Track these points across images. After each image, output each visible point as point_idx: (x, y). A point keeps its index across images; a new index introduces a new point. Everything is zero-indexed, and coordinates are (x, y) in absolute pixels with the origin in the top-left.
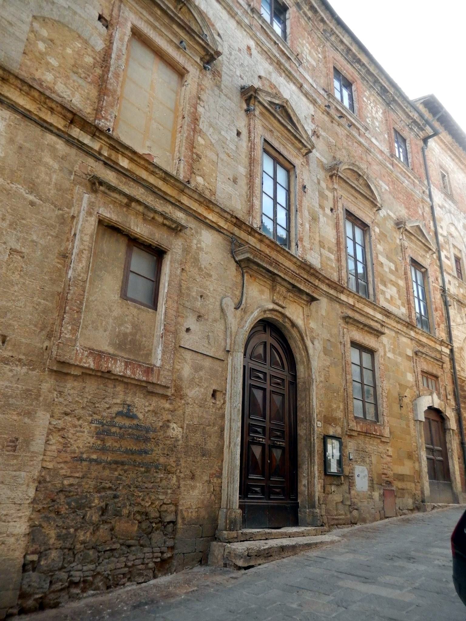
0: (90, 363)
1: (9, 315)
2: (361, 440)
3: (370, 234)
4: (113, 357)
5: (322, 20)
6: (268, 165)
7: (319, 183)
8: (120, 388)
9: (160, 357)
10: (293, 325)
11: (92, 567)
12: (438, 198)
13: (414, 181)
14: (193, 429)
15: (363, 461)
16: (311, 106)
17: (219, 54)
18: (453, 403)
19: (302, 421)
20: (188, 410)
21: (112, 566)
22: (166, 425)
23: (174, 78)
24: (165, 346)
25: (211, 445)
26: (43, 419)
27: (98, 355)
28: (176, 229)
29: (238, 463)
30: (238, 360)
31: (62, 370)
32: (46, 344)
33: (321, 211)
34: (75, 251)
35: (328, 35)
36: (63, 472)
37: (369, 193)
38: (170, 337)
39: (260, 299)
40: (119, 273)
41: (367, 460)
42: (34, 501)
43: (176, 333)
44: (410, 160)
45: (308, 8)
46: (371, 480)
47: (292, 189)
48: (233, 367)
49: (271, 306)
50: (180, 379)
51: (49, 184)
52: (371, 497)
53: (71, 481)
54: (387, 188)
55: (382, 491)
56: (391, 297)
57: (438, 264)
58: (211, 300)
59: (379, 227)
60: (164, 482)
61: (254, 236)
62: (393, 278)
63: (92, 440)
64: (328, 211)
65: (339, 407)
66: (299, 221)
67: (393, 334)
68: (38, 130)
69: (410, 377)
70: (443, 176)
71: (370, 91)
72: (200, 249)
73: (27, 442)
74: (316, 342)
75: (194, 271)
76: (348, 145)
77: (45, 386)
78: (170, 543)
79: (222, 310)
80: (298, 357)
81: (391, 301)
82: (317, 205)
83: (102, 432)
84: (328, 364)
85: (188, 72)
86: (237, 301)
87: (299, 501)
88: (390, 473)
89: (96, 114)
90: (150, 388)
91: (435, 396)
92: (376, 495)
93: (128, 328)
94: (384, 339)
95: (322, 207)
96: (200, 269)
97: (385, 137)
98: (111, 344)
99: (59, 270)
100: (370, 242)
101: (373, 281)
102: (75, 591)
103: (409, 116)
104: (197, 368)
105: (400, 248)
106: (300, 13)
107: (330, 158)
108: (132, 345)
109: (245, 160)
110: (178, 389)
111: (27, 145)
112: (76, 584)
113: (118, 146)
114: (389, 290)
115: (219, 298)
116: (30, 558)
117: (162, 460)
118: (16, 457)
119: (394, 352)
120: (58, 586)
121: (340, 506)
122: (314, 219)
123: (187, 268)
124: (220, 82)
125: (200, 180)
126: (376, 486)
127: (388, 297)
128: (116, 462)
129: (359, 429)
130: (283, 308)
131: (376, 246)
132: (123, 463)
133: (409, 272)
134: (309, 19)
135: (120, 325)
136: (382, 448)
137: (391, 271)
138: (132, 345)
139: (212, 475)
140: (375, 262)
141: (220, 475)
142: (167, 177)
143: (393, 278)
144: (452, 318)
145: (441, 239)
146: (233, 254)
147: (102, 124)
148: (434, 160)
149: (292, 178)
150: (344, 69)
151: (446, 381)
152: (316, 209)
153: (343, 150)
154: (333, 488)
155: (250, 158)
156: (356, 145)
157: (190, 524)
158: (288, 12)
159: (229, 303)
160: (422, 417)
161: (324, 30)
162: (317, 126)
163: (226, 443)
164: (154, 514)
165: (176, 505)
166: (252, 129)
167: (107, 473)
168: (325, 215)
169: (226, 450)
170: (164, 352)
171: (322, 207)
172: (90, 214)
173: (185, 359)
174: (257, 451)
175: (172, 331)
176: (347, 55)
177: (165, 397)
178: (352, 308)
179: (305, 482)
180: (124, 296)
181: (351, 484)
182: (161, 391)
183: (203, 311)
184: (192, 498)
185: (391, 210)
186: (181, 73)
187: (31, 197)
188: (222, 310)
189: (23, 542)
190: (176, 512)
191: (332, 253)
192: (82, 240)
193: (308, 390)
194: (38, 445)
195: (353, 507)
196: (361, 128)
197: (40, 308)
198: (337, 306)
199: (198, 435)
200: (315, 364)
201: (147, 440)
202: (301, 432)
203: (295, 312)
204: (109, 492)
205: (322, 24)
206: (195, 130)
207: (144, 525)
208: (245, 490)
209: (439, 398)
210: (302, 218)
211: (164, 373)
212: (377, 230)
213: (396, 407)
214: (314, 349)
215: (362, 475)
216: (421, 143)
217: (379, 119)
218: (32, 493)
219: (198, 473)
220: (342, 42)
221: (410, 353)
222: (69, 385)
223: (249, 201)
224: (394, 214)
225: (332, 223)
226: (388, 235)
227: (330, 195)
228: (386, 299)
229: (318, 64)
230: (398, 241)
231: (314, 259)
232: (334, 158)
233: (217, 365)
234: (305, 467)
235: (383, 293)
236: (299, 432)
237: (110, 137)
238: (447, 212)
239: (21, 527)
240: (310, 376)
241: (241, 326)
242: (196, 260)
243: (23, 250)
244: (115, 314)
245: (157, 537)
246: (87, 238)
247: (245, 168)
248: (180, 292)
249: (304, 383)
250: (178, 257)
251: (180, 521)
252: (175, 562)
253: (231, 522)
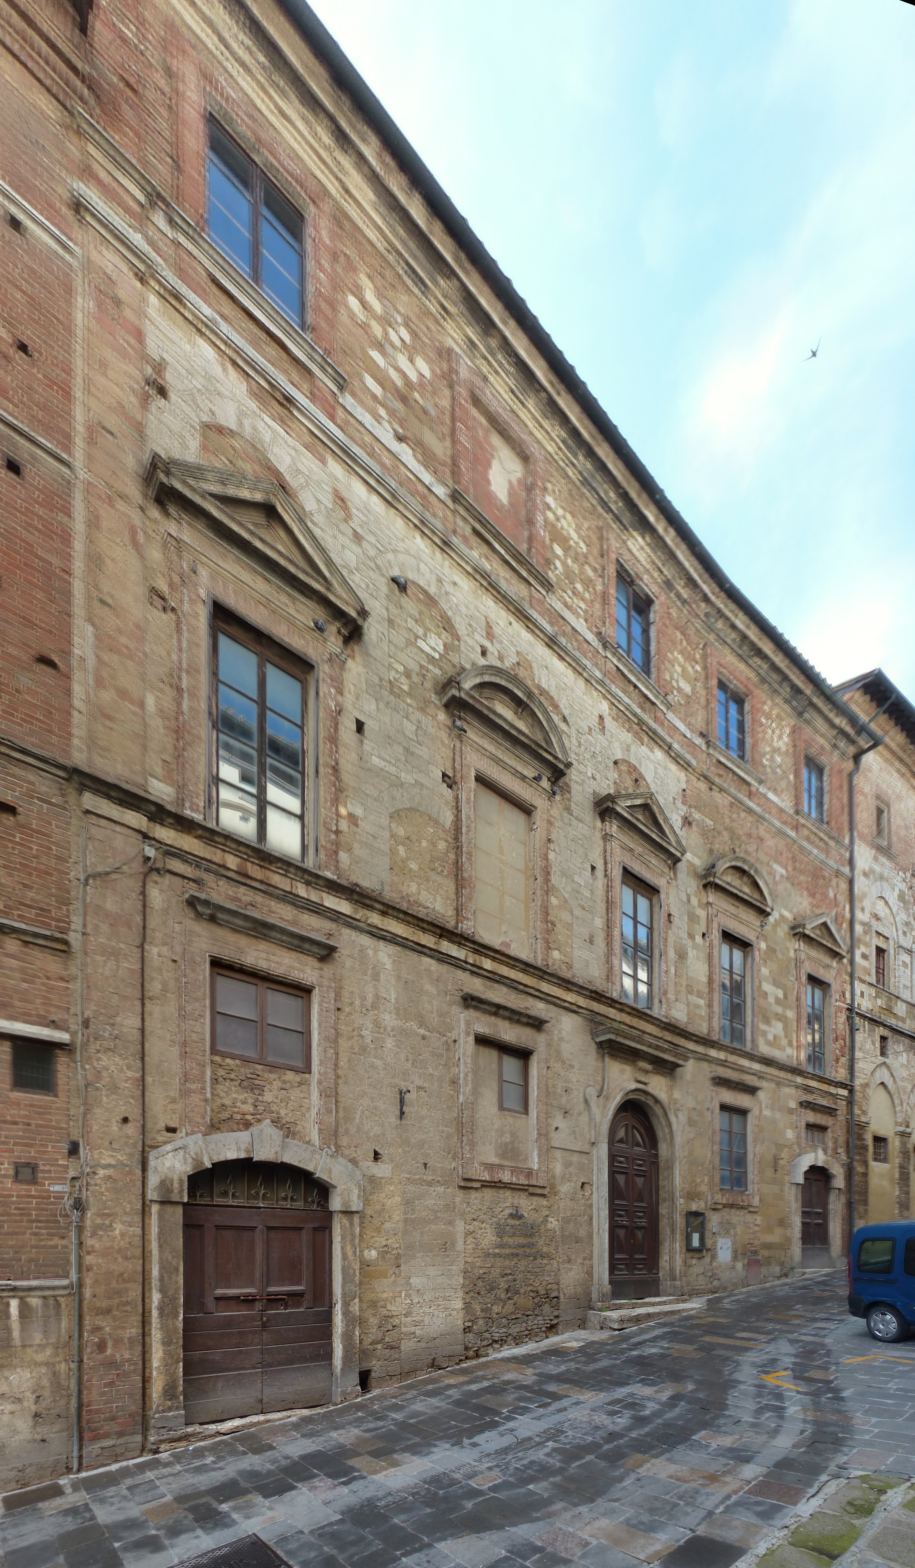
0: (486, 1176)
1: (426, 1146)
2: (726, 1214)
3: (753, 956)
4: (501, 1167)
5: (706, 599)
6: (627, 894)
7: (689, 901)
8: (508, 1193)
9: (536, 1160)
10: (657, 1101)
11: (504, 1330)
12: (864, 856)
13: (827, 844)
14: (566, 1221)
15: (727, 1232)
16: (682, 775)
17: (569, 765)
18: (844, 1157)
19: (664, 1200)
20: (562, 1205)
21: (517, 1330)
22: (545, 1220)
23: (519, 817)
24: (540, 1149)
25: (582, 1233)
26: (460, 1226)
27: (490, 1167)
28: (537, 1024)
29: (607, 1246)
30: (603, 1150)
31: (467, 1185)
32: (454, 1165)
33: (689, 943)
34: (462, 1076)
35: (713, 620)
36: (478, 1264)
37: (756, 896)
38: (543, 1140)
39: (623, 1079)
40: (495, 1085)
41: (732, 1232)
42: (463, 1286)
43: (546, 1135)
44: (826, 807)
45: (682, 583)
46: (735, 1252)
47: (655, 926)
48: (599, 1158)
49: (634, 1086)
50: (554, 1177)
51: (432, 1012)
52: (733, 1268)
53: (485, 1270)
54: (784, 872)
55: (746, 1261)
56: (775, 1037)
57: (849, 970)
58: (575, 1093)
59: (765, 941)
60: (548, 1267)
61: (613, 1007)
62: (779, 1010)
63: (494, 1238)
64: (699, 939)
65: (703, 1181)
66: (664, 968)
67: (773, 1086)
68: (414, 956)
69: (790, 1134)
70: (880, 812)
71: (772, 700)
72: (561, 1039)
73: (453, 1244)
74: (680, 1115)
75: (557, 1066)
76: (732, 820)
77: (458, 1199)
78: (556, 1313)
79: (586, 1101)
80: (660, 1134)
81: (774, 1043)
82: (686, 936)
83: (500, 1231)
84: (692, 1136)
85: (536, 808)
86: (598, 1087)
87: (660, 1274)
88: (756, 1242)
89: (457, 915)
90: (531, 1190)
91: (820, 1152)
92: (739, 1265)
93: (507, 1138)
94: (761, 1094)
95: (691, 936)
96: (563, 1062)
97: (789, 782)
98: (497, 1155)
99: (452, 1096)
100: (752, 968)
101: (752, 1022)
102: (496, 1346)
103: (833, 725)
104: (567, 1164)
105: (793, 963)
106: (670, 598)
107: (705, 856)
108: (510, 1151)
109: (601, 907)
110: (553, 1187)
111: (410, 977)
112: (496, 1342)
113: (482, 949)
114: (772, 1029)
115: (582, 1089)
116: (467, 1324)
117: (545, 1249)
118: (448, 1256)
119: (772, 1108)
120: (485, 1343)
121: (701, 1278)
122: (682, 956)
123: (551, 1064)
124: (569, 800)
125: (556, 954)
126: (739, 1257)
127: (770, 1037)
128: (513, 1254)
129: (724, 1202)
130: (645, 1084)
131: (759, 970)
132: (517, 1255)
133: (803, 996)
134: (684, 602)
135: (502, 1136)
136: (749, 1217)
137: (778, 1001)
138: (510, 1151)
139: (585, 1259)
140: (756, 995)
141: (591, 1259)
142: (527, 967)
143: (779, 1010)
144: (858, 1045)
145: (858, 929)
146: (594, 1034)
147: (466, 927)
148: (867, 789)
149: (656, 909)
150: (735, 678)
151: (837, 1129)
152: (684, 942)
153: (725, 833)
154: (694, 1261)
155: (607, 902)
156: (743, 814)
157: (570, 1298)
158: (652, 609)
159: (592, 1092)
160: (801, 1180)
161: (707, 615)
162: (690, 807)
163: (595, 1230)
164: (543, 1292)
165: (558, 1284)
166: (608, 857)
167: (507, 1262)
168: (695, 946)
169: (595, 1236)
170: (539, 1156)
171: (691, 936)
172: (468, 1034)
173: (555, 1158)
174: (621, 1233)
175: (543, 1134)
176: (740, 647)
177: (544, 1196)
178: (723, 1063)
179: (666, 1258)
180: (501, 1108)
181: (714, 1257)
182: (539, 1191)
183: (568, 1107)
184: (570, 1279)
185: (786, 908)
186: (527, 810)
187: (422, 1031)
188: (586, 1101)
189: (461, 1314)
190: (558, 1289)
191: (702, 998)
192: (465, 1063)
193: (670, 1168)
194: (460, 1245)
195: (713, 1277)
196: (753, 782)
197: (445, 1135)
198: (705, 1065)
199: (571, 1225)
200: (678, 1139)
201: (531, 1235)
202: (663, 1210)
203: (657, 1085)
204: (510, 1277)
205: (703, 605)
206: (548, 890)
207: (536, 1300)
208: (612, 1269)
209: (825, 1153)
210: (666, 963)
211: (541, 1175)
212: (763, 945)
213: (769, 1173)
214: (678, 1122)
215: (725, 1247)
216: (849, 765)
217: (784, 749)
218: (461, 1281)
219: (573, 1257)
220: (733, 627)
221: (793, 1105)
222: (473, 1197)
223: (607, 962)
224: (791, 912)
225: (703, 955)
226: (778, 949)
227: (702, 913)
228: (768, 1043)
229: (694, 688)
230: (792, 954)
231: (679, 1014)
232: (711, 851)
233: (584, 1159)
234: (667, 1244)
235: (764, 1033)
236: (661, 1210)
237: (474, 942)
238: (876, 880)
239: (459, 1304)
240: (673, 1153)
241: (604, 1114)
242: (558, 1052)
243: (425, 1085)
244: (496, 1126)
245: (546, 1308)
246: (469, 1060)
247: (602, 917)
248: (547, 1092)
249: (667, 1161)
250: (543, 1056)
251: (562, 1296)
252: (560, 1327)
253: (603, 1295)
